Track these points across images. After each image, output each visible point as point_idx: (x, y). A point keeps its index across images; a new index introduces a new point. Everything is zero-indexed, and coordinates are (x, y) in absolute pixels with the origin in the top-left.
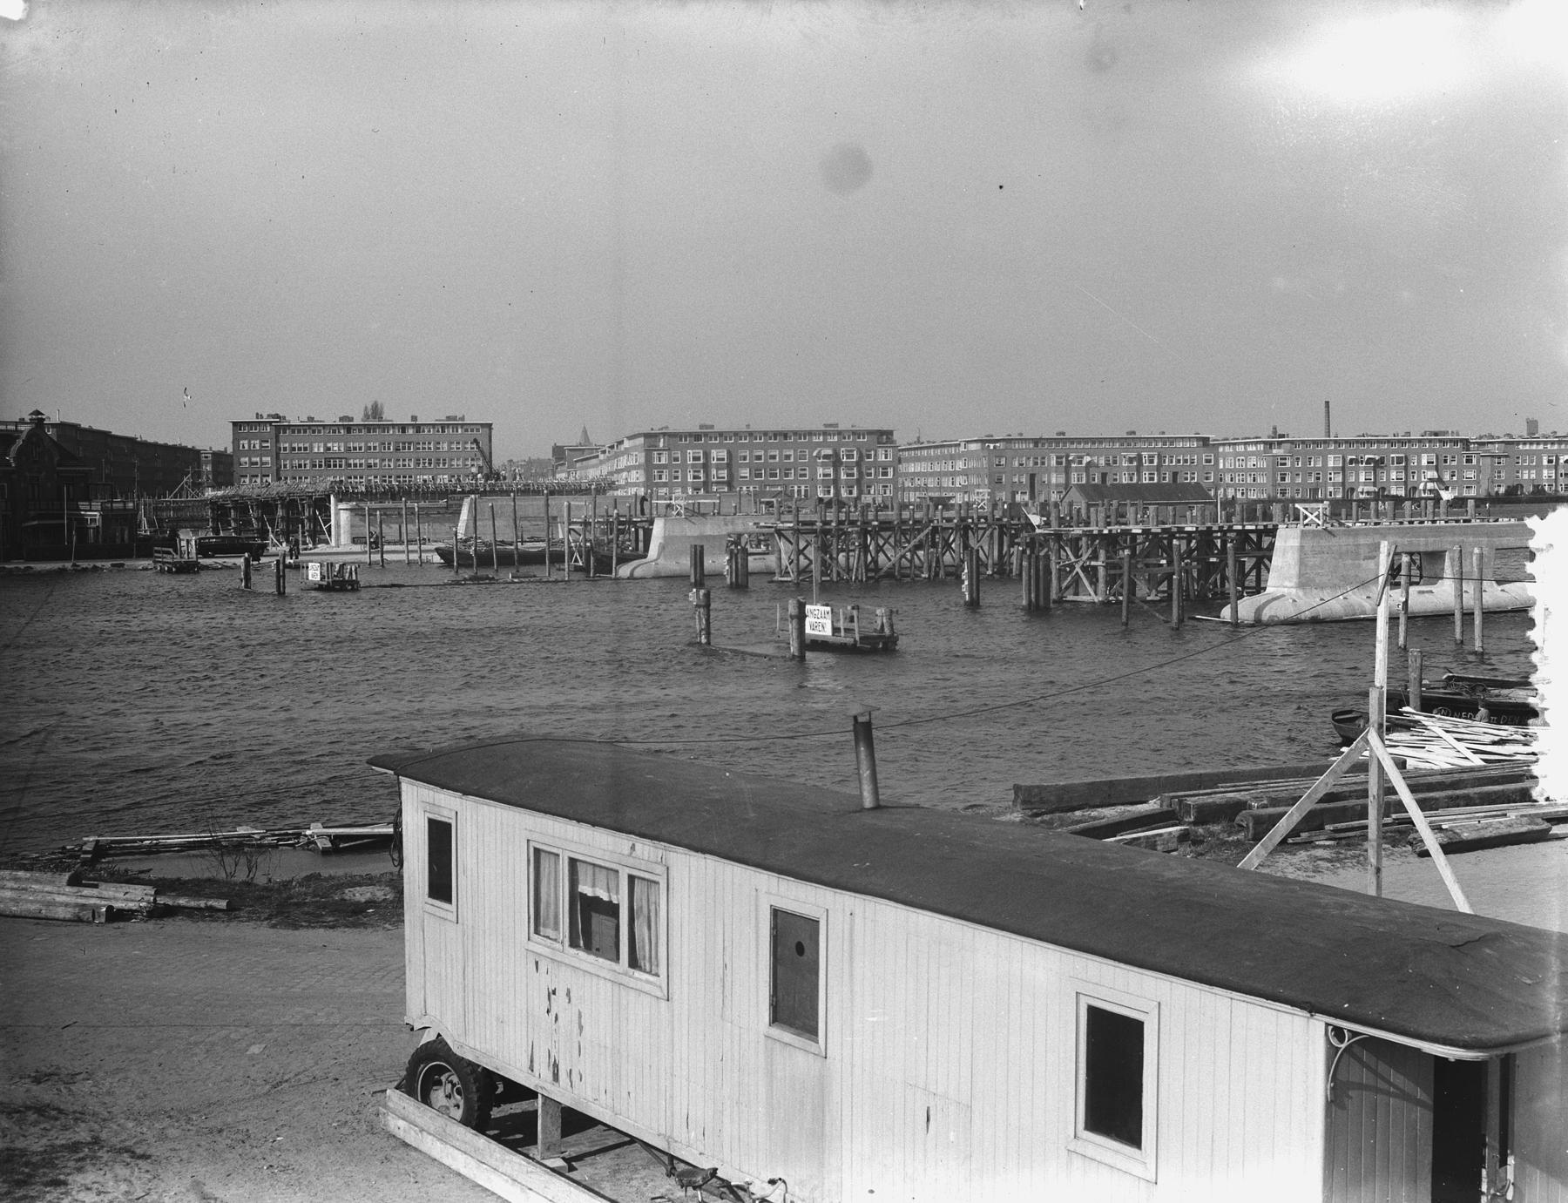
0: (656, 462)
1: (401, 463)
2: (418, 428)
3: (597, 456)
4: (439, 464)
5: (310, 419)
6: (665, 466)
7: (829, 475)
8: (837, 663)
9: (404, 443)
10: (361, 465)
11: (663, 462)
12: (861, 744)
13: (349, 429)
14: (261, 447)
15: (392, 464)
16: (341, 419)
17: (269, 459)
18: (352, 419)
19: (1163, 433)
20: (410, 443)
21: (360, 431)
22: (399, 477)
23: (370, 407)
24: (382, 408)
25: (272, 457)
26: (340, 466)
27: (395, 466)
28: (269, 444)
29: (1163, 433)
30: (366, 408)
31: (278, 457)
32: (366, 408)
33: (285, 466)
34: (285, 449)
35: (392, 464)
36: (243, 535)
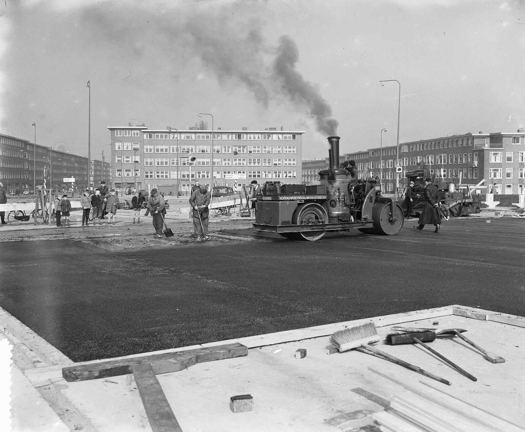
0: (493, 161)
4: (250, 163)
6: (499, 165)
11: (498, 161)
22: (147, 173)
35: (230, 163)
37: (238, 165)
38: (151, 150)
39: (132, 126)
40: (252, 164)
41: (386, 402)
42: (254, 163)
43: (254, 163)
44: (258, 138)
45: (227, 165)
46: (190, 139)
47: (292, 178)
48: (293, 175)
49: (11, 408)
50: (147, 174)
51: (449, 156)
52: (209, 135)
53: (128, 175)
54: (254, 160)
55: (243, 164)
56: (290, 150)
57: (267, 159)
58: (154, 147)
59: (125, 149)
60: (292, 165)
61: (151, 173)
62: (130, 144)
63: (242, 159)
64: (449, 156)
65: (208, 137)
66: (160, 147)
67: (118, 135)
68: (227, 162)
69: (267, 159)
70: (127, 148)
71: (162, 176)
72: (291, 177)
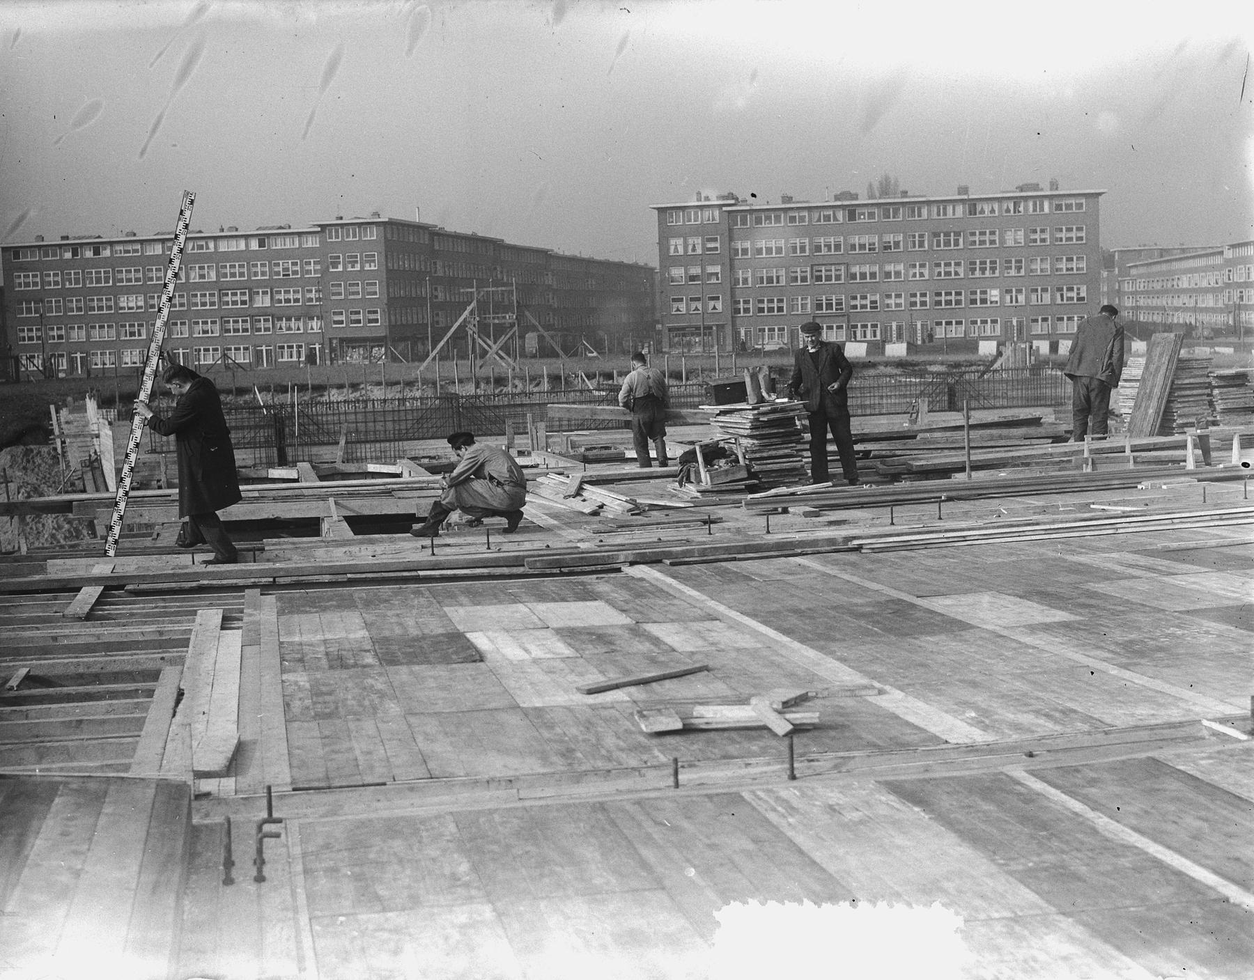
1: (942, 270)
2: (972, 206)
3: (1221, 253)
4: (973, 270)
5: (787, 199)
7: (1083, 269)
8: (74, 393)
9: (947, 234)
10: (873, 275)
12: (1179, 704)
13: (852, 212)
14: (705, 249)
15: (926, 272)
16: (837, 198)
17: (718, 269)
18: (855, 197)
19: (341, 218)
20: (957, 234)
21: (778, 219)
22: (939, 294)
23: (876, 185)
24: (897, 181)
25: (723, 265)
26: (838, 278)
27: (931, 275)
28: (718, 245)
29: (341, 218)
30: (870, 185)
31: (732, 267)
32: (870, 185)
33: (745, 281)
34: (745, 251)
35: (926, 272)
36: (1102, 469)
37: (943, 277)
38: (838, 247)
39: (1042, 190)
40: (978, 274)
41: (376, 908)
42: (983, 270)
43: (983, 270)
44: (993, 211)
45: (918, 278)
46: (832, 222)
47: (859, 310)
48: (1078, 294)
49: (847, 903)
50: (973, 297)
51: (926, 245)
52: (1083, 201)
53: (714, 308)
54: (981, 263)
55: (956, 273)
56: (1069, 235)
57: (988, 261)
58: (845, 240)
59: (690, 252)
60: (1075, 272)
61: (958, 294)
62: (698, 241)
63: (953, 263)
64: (926, 245)
65: (1079, 206)
66: (856, 240)
67: (690, 220)
68: (917, 270)
69: (988, 261)
70: (694, 249)
71: (771, 310)
72: (1072, 299)
